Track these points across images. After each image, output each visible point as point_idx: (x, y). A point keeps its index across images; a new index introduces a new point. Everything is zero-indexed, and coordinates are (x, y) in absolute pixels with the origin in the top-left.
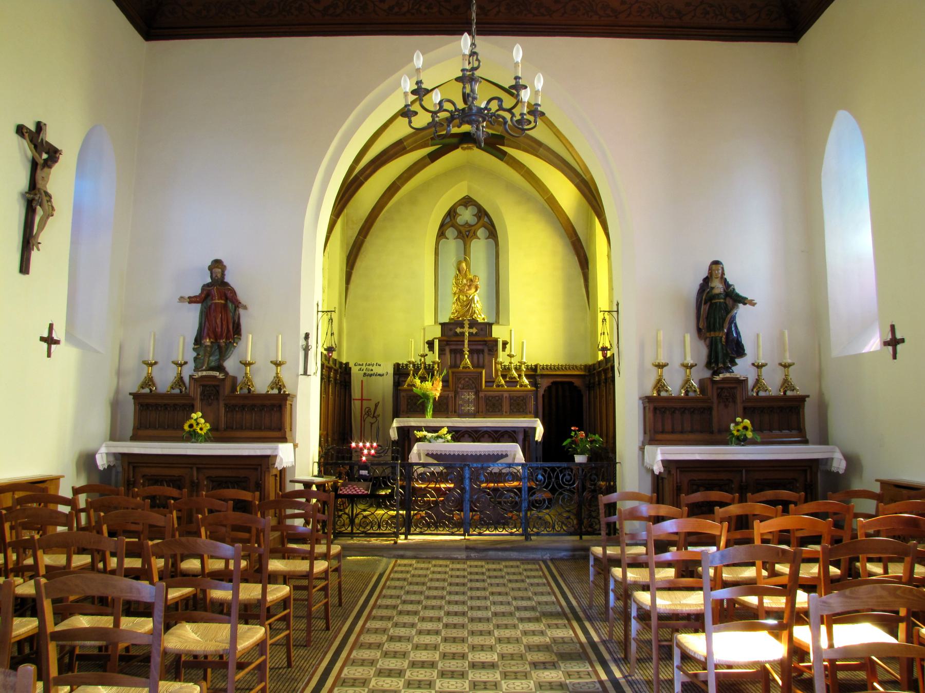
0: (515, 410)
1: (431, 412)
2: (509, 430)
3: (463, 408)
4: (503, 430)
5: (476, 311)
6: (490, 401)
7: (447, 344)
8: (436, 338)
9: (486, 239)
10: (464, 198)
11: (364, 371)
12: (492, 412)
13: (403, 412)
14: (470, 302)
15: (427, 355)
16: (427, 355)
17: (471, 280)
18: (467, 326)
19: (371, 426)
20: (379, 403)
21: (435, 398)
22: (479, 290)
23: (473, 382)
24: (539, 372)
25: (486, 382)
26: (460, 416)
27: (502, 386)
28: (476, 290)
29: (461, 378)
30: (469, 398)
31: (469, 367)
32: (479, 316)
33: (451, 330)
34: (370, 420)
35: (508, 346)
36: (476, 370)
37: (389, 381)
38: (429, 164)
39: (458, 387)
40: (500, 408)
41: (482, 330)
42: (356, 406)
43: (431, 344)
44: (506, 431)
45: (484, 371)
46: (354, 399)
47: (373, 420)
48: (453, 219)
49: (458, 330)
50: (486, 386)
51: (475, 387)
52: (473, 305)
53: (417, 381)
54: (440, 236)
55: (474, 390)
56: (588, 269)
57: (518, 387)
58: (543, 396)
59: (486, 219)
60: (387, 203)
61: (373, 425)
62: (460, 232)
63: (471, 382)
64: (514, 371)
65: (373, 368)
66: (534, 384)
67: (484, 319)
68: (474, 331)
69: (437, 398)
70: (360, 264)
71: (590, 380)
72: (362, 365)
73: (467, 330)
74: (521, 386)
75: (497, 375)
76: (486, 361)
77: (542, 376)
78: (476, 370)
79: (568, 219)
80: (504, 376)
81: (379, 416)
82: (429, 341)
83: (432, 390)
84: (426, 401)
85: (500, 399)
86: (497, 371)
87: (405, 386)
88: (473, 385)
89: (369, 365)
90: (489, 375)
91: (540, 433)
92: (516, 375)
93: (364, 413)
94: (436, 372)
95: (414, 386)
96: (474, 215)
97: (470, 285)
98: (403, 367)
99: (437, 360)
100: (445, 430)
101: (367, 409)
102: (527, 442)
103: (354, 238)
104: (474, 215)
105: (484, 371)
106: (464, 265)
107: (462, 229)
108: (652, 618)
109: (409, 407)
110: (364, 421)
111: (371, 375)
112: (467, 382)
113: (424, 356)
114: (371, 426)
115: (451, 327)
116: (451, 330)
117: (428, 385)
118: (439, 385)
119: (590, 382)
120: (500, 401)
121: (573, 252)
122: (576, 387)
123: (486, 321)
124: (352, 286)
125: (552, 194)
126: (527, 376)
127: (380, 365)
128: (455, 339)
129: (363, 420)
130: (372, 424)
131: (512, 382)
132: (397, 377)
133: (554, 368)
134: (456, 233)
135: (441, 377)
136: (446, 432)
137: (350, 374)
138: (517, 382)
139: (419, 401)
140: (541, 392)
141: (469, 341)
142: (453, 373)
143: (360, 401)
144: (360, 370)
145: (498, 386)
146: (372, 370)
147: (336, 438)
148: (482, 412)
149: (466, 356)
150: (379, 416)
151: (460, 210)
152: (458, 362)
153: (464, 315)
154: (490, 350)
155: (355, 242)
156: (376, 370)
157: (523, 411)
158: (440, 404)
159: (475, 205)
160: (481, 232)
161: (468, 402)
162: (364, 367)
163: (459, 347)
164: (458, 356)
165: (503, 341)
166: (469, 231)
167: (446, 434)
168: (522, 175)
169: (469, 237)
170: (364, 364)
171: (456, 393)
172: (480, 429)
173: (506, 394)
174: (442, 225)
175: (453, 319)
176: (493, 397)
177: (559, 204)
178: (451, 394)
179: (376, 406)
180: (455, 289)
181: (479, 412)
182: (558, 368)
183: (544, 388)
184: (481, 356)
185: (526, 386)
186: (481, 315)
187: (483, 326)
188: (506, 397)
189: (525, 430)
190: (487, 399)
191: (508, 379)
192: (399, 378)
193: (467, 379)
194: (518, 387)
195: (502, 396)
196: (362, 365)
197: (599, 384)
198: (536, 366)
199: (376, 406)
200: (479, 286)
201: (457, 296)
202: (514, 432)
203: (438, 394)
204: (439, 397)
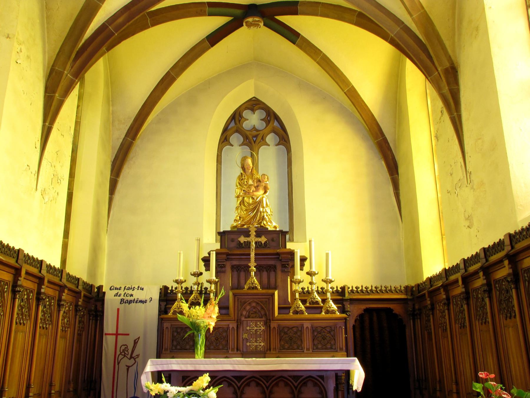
0: (320, 346)
1: (204, 349)
2: (314, 375)
3: (248, 344)
4: (306, 375)
5: (265, 216)
6: (286, 333)
7: (227, 259)
8: (213, 251)
9: (276, 145)
10: (250, 100)
11: (122, 297)
12: (288, 349)
13: (166, 350)
14: (257, 205)
15: (201, 274)
16: (201, 274)
17: (259, 181)
18: (253, 233)
19: (128, 370)
20: (139, 338)
21: (209, 329)
22: (268, 191)
23: (263, 308)
24: (347, 296)
25: (279, 308)
26: (244, 355)
27: (302, 312)
28: (265, 192)
29: (245, 303)
30: (256, 330)
31: (256, 288)
32: (269, 223)
33: (233, 240)
34: (126, 362)
35: (307, 263)
36: (264, 291)
37: (153, 308)
38: (209, 48)
39: (241, 315)
40: (299, 343)
41: (273, 240)
42: (109, 343)
43: (206, 261)
44: (310, 376)
45: (276, 293)
46: (106, 334)
47: (131, 362)
48: (238, 122)
49: (242, 239)
50: (279, 314)
51: (266, 315)
52: (261, 209)
53: (185, 306)
54: (223, 142)
55: (264, 319)
56: (398, 174)
57: (323, 313)
58: (354, 326)
59: (276, 124)
60: (159, 98)
61: (130, 369)
62: (246, 137)
63: (259, 308)
64: (315, 294)
65: (133, 293)
66: (342, 310)
67: (275, 227)
68: (263, 240)
69: (211, 329)
70: (127, 171)
71: (414, 305)
72: (120, 289)
73: (253, 240)
74: (327, 312)
75: (294, 299)
76: (279, 280)
77: (352, 301)
78: (264, 291)
79: (373, 116)
80: (304, 302)
81: (138, 356)
82: (205, 257)
83: (204, 317)
84: (196, 333)
85: (299, 330)
86: (293, 293)
87: (170, 314)
88: (263, 313)
89: (129, 289)
90: (283, 299)
91: (359, 380)
92: (319, 299)
93: (118, 353)
94: (212, 295)
95: (181, 313)
96: (262, 120)
97: (258, 186)
98: (172, 291)
99: (214, 278)
100: (205, 380)
101: (123, 347)
102: (340, 393)
103: (121, 140)
104: (262, 120)
105: (276, 293)
106: (249, 161)
107: (248, 133)
108: (201, 260)
109: (175, 343)
110: (118, 363)
111: (130, 302)
112: (254, 307)
113: (198, 274)
114: (128, 370)
115: (232, 236)
116: (233, 240)
117: (199, 311)
118: (214, 311)
119: (414, 308)
120: (299, 334)
121: (380, 156)
122: (396, 315)
123: (278, 229)
124: (117, 196)
125: (353, 87)
126: (335, 301)
127: (142, 289)
128: (238, 252)
129: (116, 362)
130: (128, 367)
131: (314, 308)
132: (164, 304)
133: (367, 291)
134: (242, 139)
135: (218, 300)
136: (205, 384)
137: (103, 301)
138: (322, 307)
139: (187, 332)
140: (351, 323)
141: (256, 254)
142: (235, 295)
143: (115, 336)
144: (116, 295)
145: (296, 312)
146: (132, 295)
147: (71, 389)
148: (275, 349)
149: (253, 274)
150: (138, 356)
151: (246, 114)
152: (242, 281)
153: (250, 222)
154: (284, 266)
155: (122, 145)
156: (137, 295)
157: (331, 348)
158: (217, 339)
159: (262, 109)
160: (270, 138)
161: (256, 335)
162: (122, 292)
163: (243, 263)
164: (242, 274)
165: (300, 256)
166: (256, 136)
167: (208, 387)
168: (318, 63)
169: (257, 142)
170: (123, 288)
171: (239, 323)
172: (273, 374)
173: (307, 324)
174: (225, 130)
175: (236, 227)
176: (289, 328)
177: (361, 98)
178: (233, 325)
179: (136, 342)
180: (238, 191)
181: (270, 350)
182: (367, 291)
183: (355, 318)
184: (272, 274)
185: (333, 312)
186: (271, 222)
187: (275, 236)
188: (307, 327)
189: (337, 375)
190: (283, 331)
191: (308, 304)
192: (166, 305)
193: (254, 304)
194: (323, 313)
195: (302, 326)
196: (120, 289)
197: (433, 308)
198: (343, 288)
199: (136, 342)
200: (269, 187)
201: (241, 198)
202: (322, 377)
203: (212, 325)
204: (214, 328)
